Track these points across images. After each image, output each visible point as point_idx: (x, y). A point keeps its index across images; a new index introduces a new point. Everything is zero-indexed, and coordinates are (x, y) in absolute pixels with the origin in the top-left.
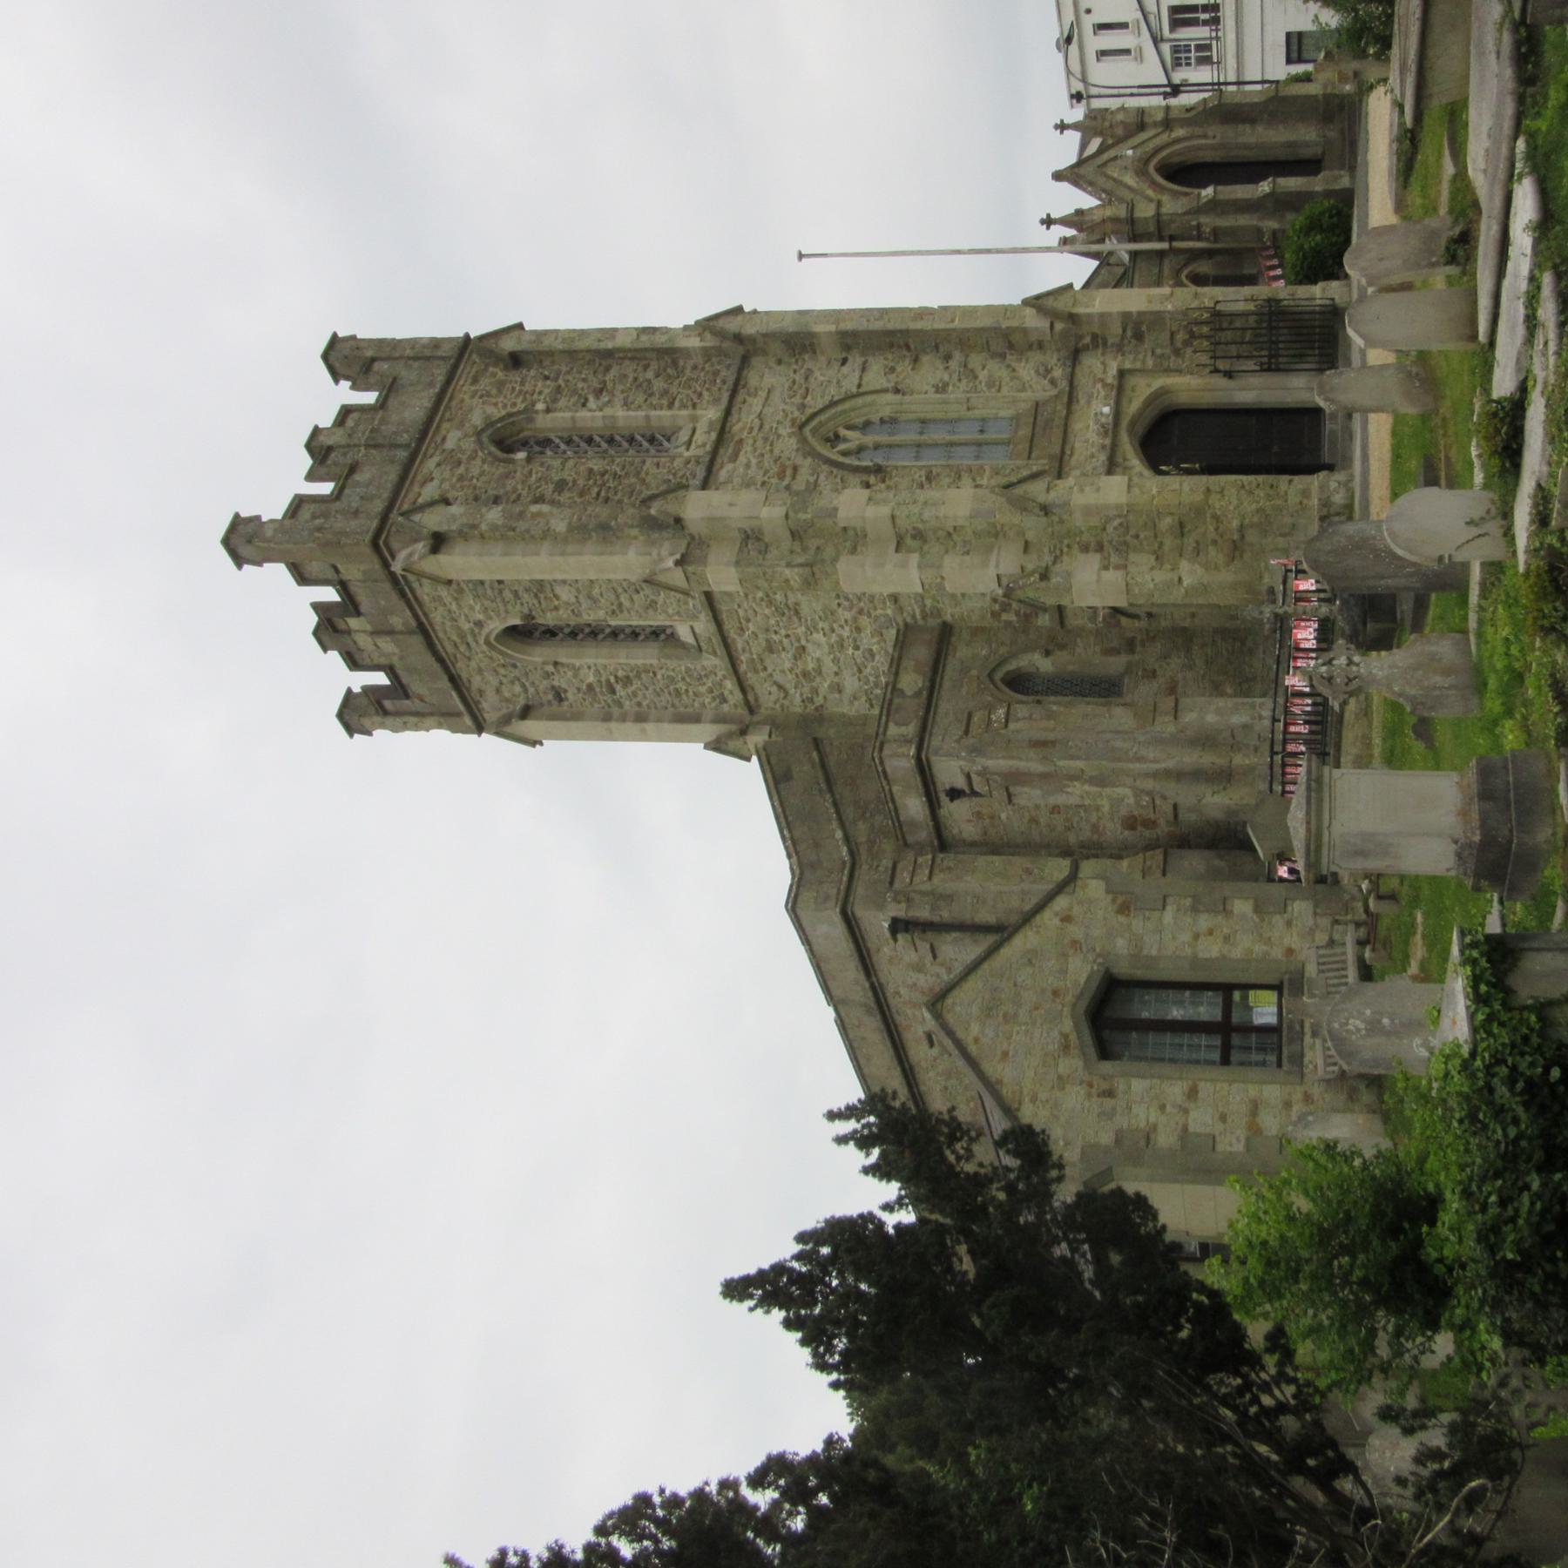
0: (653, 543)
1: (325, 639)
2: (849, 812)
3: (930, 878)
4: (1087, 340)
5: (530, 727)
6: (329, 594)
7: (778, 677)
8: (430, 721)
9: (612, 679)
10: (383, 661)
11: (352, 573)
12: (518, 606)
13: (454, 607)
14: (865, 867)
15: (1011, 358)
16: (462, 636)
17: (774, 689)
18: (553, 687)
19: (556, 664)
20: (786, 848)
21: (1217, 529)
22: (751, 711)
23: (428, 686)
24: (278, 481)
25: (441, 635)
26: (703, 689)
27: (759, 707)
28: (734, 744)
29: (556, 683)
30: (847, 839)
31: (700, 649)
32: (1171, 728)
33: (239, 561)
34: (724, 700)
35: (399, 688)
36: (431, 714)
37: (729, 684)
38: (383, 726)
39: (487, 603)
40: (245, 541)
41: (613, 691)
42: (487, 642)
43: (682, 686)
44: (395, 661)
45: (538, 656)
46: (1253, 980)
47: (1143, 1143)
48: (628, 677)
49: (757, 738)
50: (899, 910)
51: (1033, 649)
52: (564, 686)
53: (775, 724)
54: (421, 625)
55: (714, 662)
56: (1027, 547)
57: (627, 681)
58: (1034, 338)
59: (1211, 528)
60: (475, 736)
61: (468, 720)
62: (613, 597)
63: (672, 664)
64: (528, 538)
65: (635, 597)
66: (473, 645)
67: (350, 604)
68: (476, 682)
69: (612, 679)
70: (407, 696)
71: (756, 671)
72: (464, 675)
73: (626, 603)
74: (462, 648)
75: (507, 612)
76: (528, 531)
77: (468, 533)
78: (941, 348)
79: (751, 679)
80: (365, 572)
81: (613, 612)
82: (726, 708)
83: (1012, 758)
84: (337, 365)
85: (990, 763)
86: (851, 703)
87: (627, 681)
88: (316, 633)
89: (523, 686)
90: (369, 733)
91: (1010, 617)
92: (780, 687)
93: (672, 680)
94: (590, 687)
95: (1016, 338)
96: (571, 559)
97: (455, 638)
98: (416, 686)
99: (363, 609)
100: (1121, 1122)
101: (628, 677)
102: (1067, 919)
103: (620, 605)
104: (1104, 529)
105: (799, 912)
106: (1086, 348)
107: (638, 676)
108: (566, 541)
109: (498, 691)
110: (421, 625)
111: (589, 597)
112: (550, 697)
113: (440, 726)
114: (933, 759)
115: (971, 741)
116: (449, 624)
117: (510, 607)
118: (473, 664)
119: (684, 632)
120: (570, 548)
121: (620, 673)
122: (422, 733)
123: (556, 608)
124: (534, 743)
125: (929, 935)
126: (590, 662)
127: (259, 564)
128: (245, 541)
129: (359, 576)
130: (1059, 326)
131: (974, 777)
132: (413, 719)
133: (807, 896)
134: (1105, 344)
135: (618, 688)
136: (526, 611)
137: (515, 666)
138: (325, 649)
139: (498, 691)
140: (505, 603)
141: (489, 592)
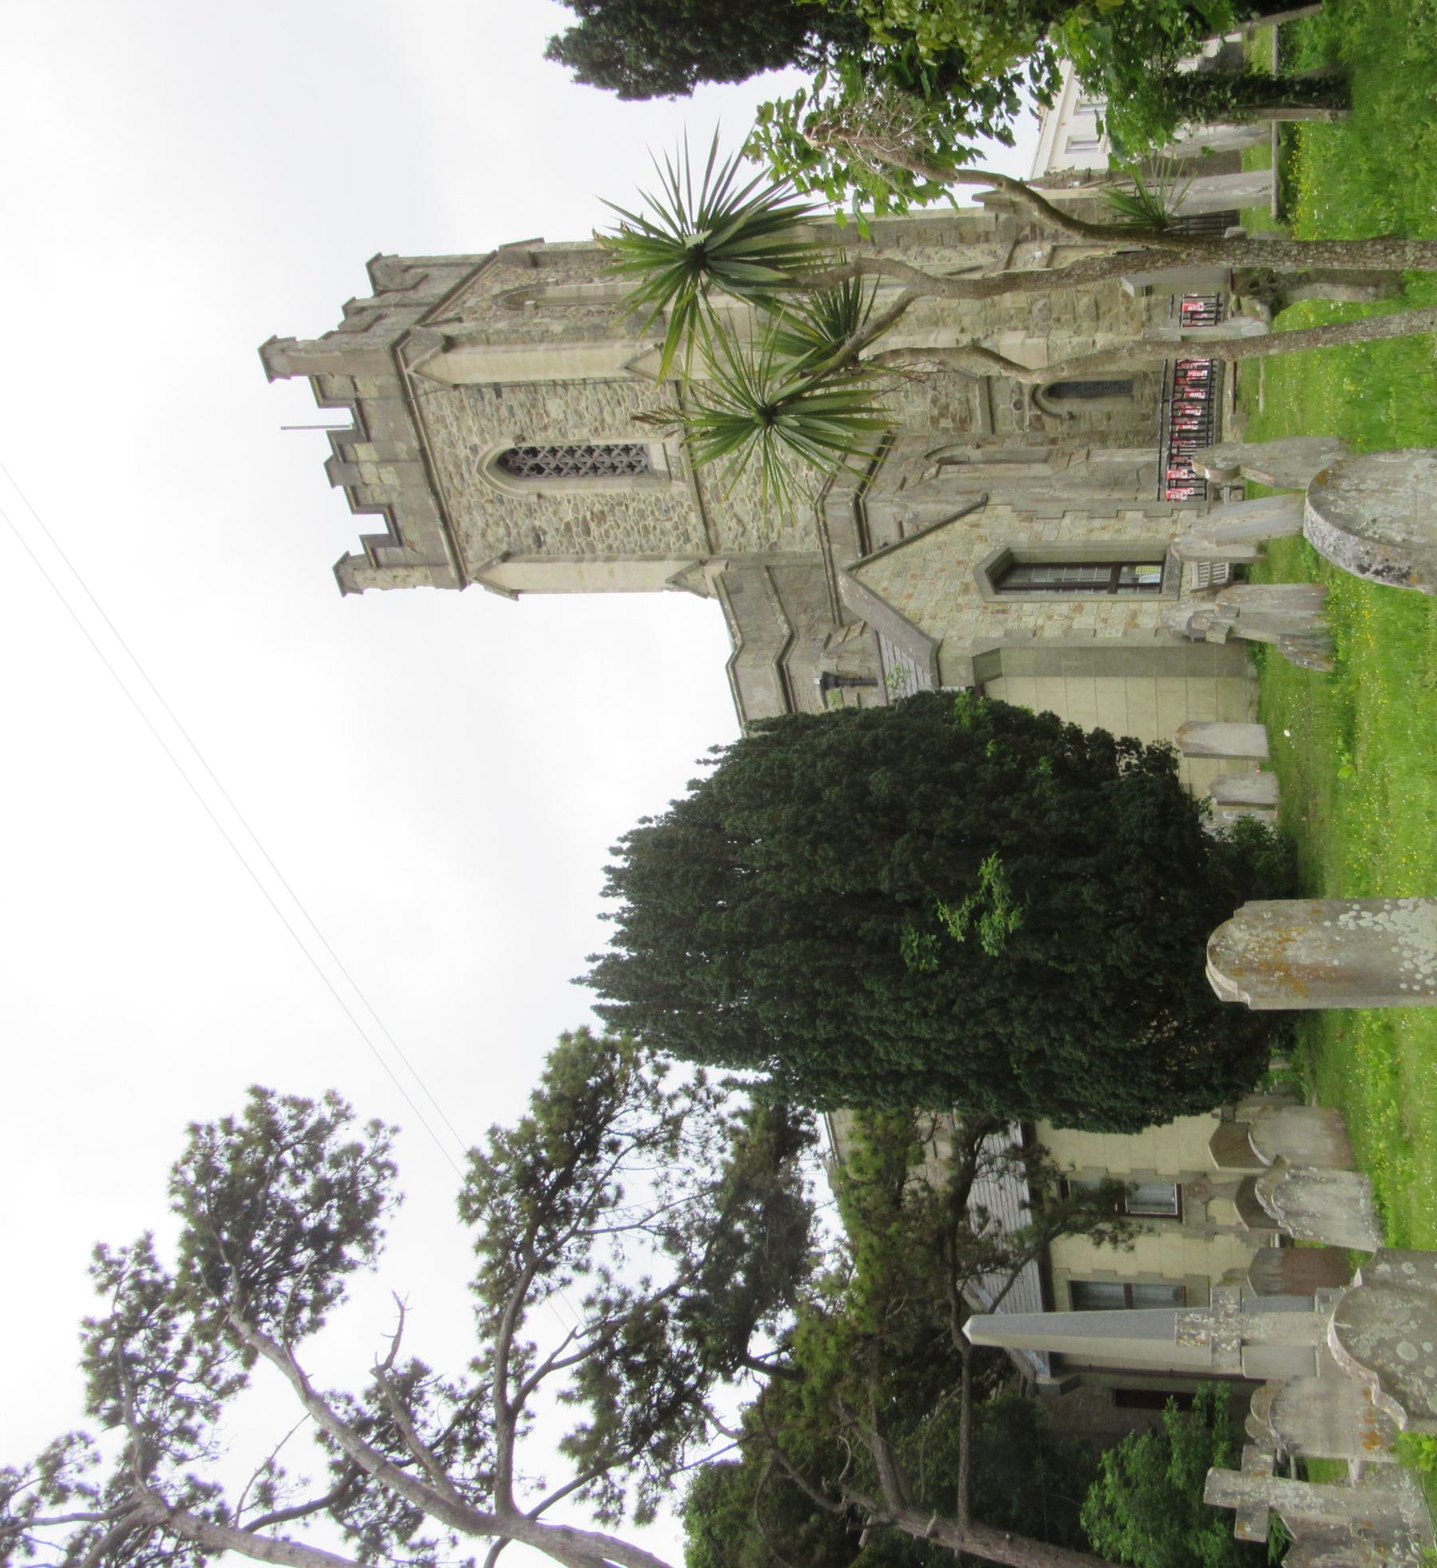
0: (637, 339)
1: (335, 471)
2: (792, 609)
3: (861, 633)
4: (1027, 231)
5: (510, 573)
6: (343, 417)
7: (738, 509)
8: (418, 574)
9: (589, 517)
10: (383, 499)
11: (368, 389)
12: (512, 426)
13: (454, 430)
14: (802, 639)
15: (962, 248)
16: (458, 466)
17: (733, 524)
18: (534, 528)
19: (539, 496)
20: (730, 626)
21: (1128, 309)
22: (712, 551)
23: (422, 532)
24: (314, 319)
25: (439, 464)
26: (668, 525)
27: (719, 547)
28: (693, 578)
29: (537, 523)
30: (788, 621)
31: (670, 476)
32: (1083, 472)
33: (272, 374)
34: (688, 540)
35: (396, 536)
36: (421, 565)
37: (694, 518)
38: (373, 583)
39: (484, 422)
40: (278, 358)
41: (587, 532)
42: (479, 471)
43: (650, 522)
44: (395, 498)
45: (523, 490)
46: (1139, 559)
47: (1030, 635)
48: (602, 512)
49: (715, 569)
50: (827, 665)
51: (966, 444)
52: (545, 526)
53: (730, 561)
54: (423, 450)
55: (681, 489)
56: (962, 331)
57: (601, 517)
58: (981, 229)
59: (1123, 309)
60: (457, 591)
61: (452, 572)
62: (597, 411)
63: (643, 493)
64: (528, 339)
65: (617, 410)
66: (467, 476)
67: (363, 429)
68: (465, 522)
69: (589, 517)
70: (401, 543)
71: (718, 500)
72: (454, 514)
73: (608, 419)
74: (456, 481)
75: (501, 433)
76: (529, 332)
77: (472, 340)
78: (902, 243)
79: (715, 509)
80: (380, 388)
81: (596, 430)
82: (689, 548)
83: (941, 502)
84: (378, 274)
85: (919, 508)
86: (802, 540)
87: (601, 517)
88: (328, 465)
89: (507, 527)
90: (359, 591)
91: (945, 423)
92: (739, 521)
93: (642, 514)
94: (568, 525)
95: (966, 229)
96: (564, 354)
97: (451, 468)
98: (411, 534)
99: (373, 434)
100: (1011, 625)
101: (602, 512)
102: (976, 526)
103: (603, 421)
104: (1030, 312)
105: (738, 669)
106: (1025, 240)
107: (612, 510)
108: (561, 341)
109: (483, 535)
110: (423, 450)
111: (577, 412)
112: (530, 541)
113: (425, 582)
114: (870, 505)
115: (904, 493)
116: (447, 450)
117: (504, 427)
118: (464, 501)
119: (657, 462)
120: (565, 346)
121: (597, 508)
122: (410, 590)
123: (545, 428)
124: (514, 593)
125: (857, 689)
126: (572, 495)
127: (287, 377)
128: (278, 358)
129: (375, 393)
130: (1003, 217)
131: (905, 524)
132: (402, 572)
133: (746, 660)
134: (1042, 234)
135: (593, 526)
136: (518, 432)
137: (501, 501)
138: (333, 485)
139: (483, 535)
140: (500, 421)
141: (488, 409)
